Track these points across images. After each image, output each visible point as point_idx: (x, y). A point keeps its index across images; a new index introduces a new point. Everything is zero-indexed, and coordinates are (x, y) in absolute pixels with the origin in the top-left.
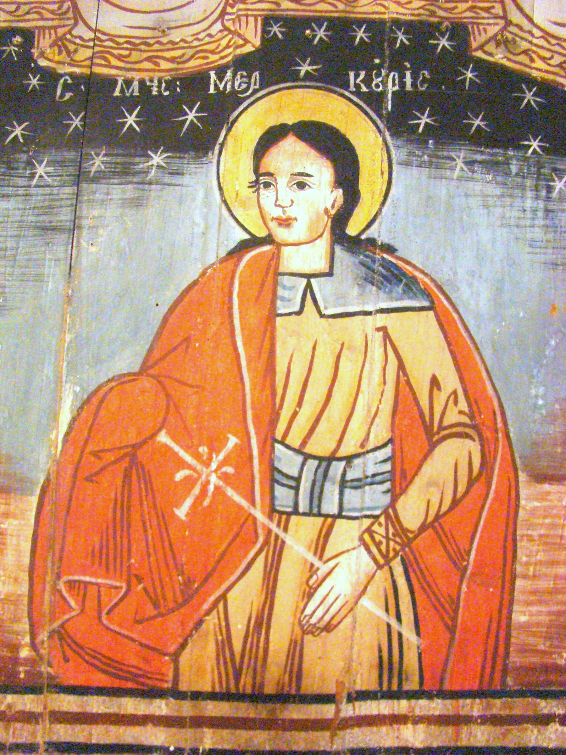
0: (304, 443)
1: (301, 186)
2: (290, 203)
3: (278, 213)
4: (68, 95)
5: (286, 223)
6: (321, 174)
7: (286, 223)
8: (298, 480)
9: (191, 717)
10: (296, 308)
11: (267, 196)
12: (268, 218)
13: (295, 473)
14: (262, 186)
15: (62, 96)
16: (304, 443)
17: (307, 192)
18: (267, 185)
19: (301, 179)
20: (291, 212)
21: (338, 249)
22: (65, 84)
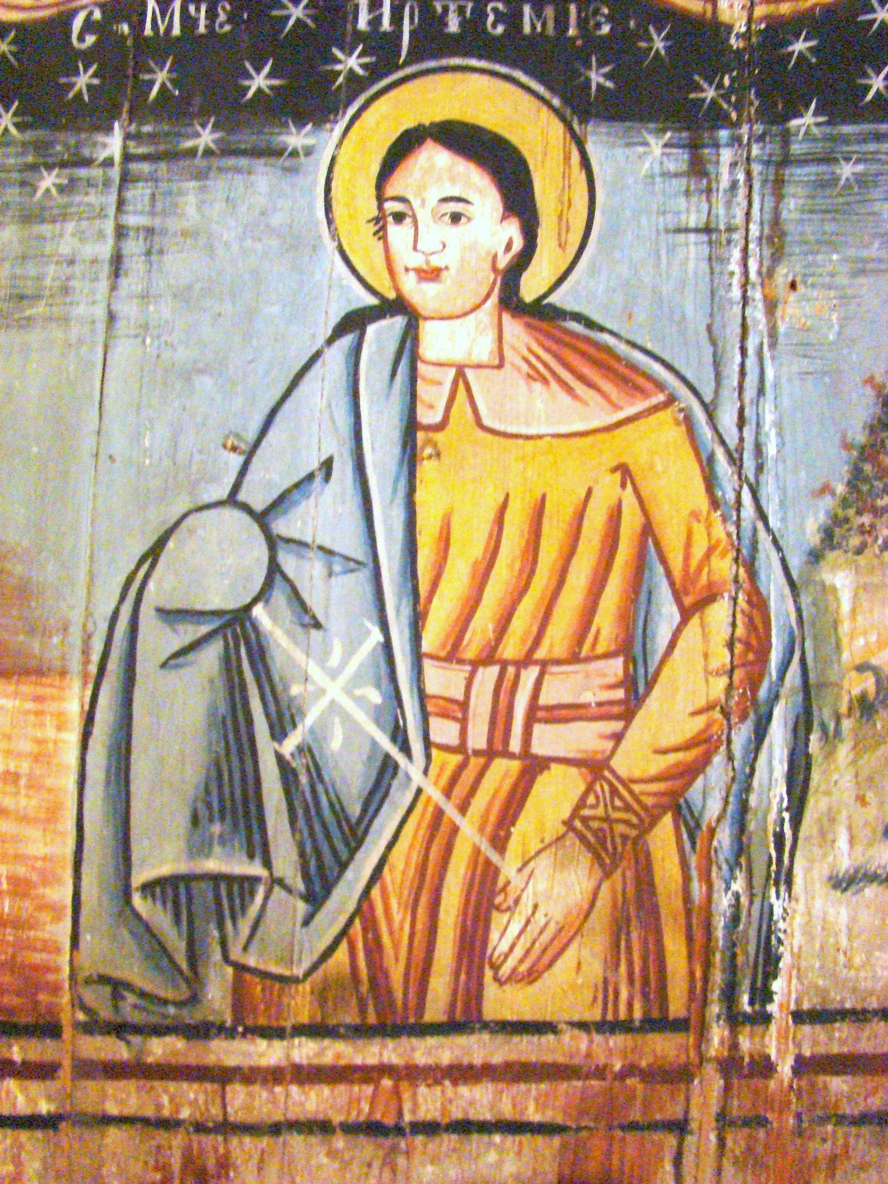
0: (281, 502)
1: (456, 218)
2: (441, 247)
3: (417, 261)
4: (90, 40)
5: (431, 274)
6: (151, 266)
7: (431, 274)
8: (464, 705)
9: (233, 1038)
10: (487, 422)
11: (398, 234)
12: (399, 268)
13: (461, 697)
14: (390, 219)
15: (81, 39)
16: (281, 502)
17: (462, 228)
18: (399, 218)
19: (453, 207)
20: (436, 261)
21: (506, 317)
22: (88, 22)
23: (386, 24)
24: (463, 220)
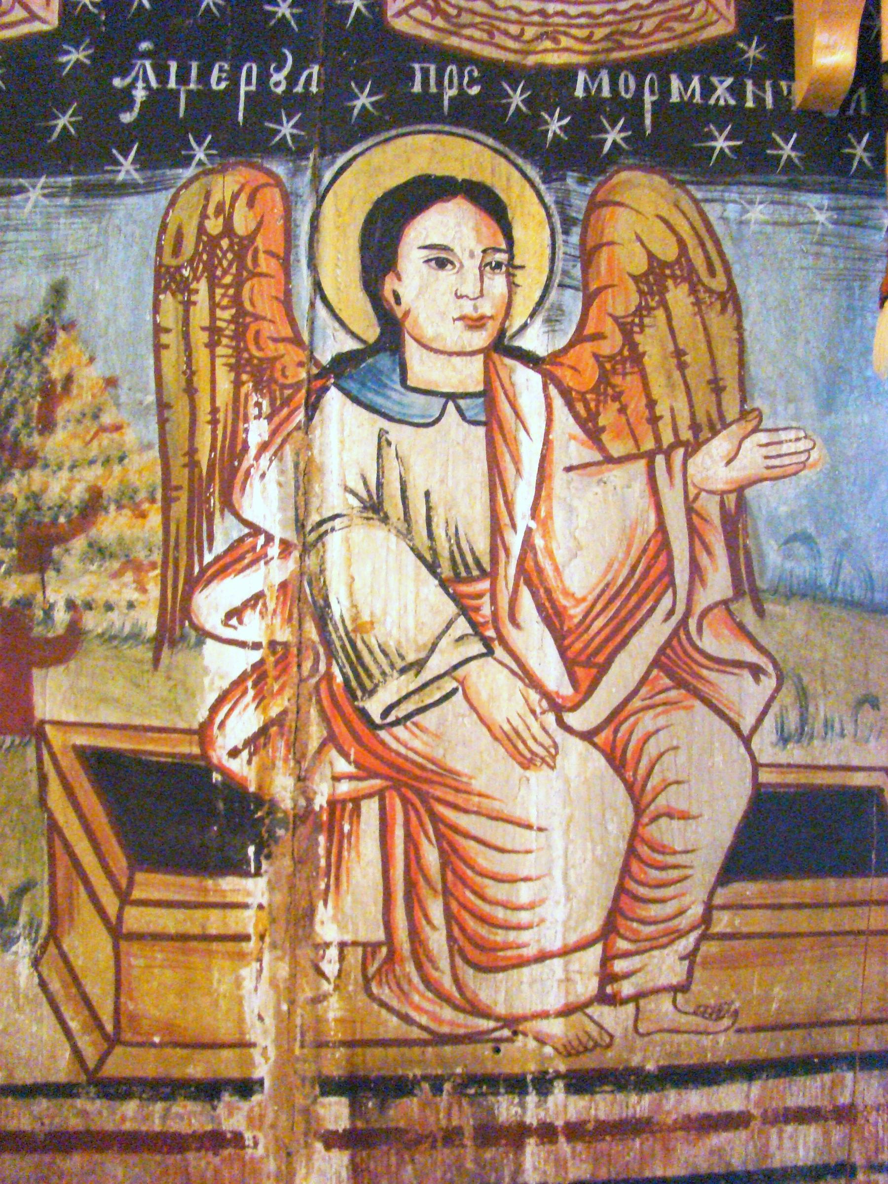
23: (433, 89)
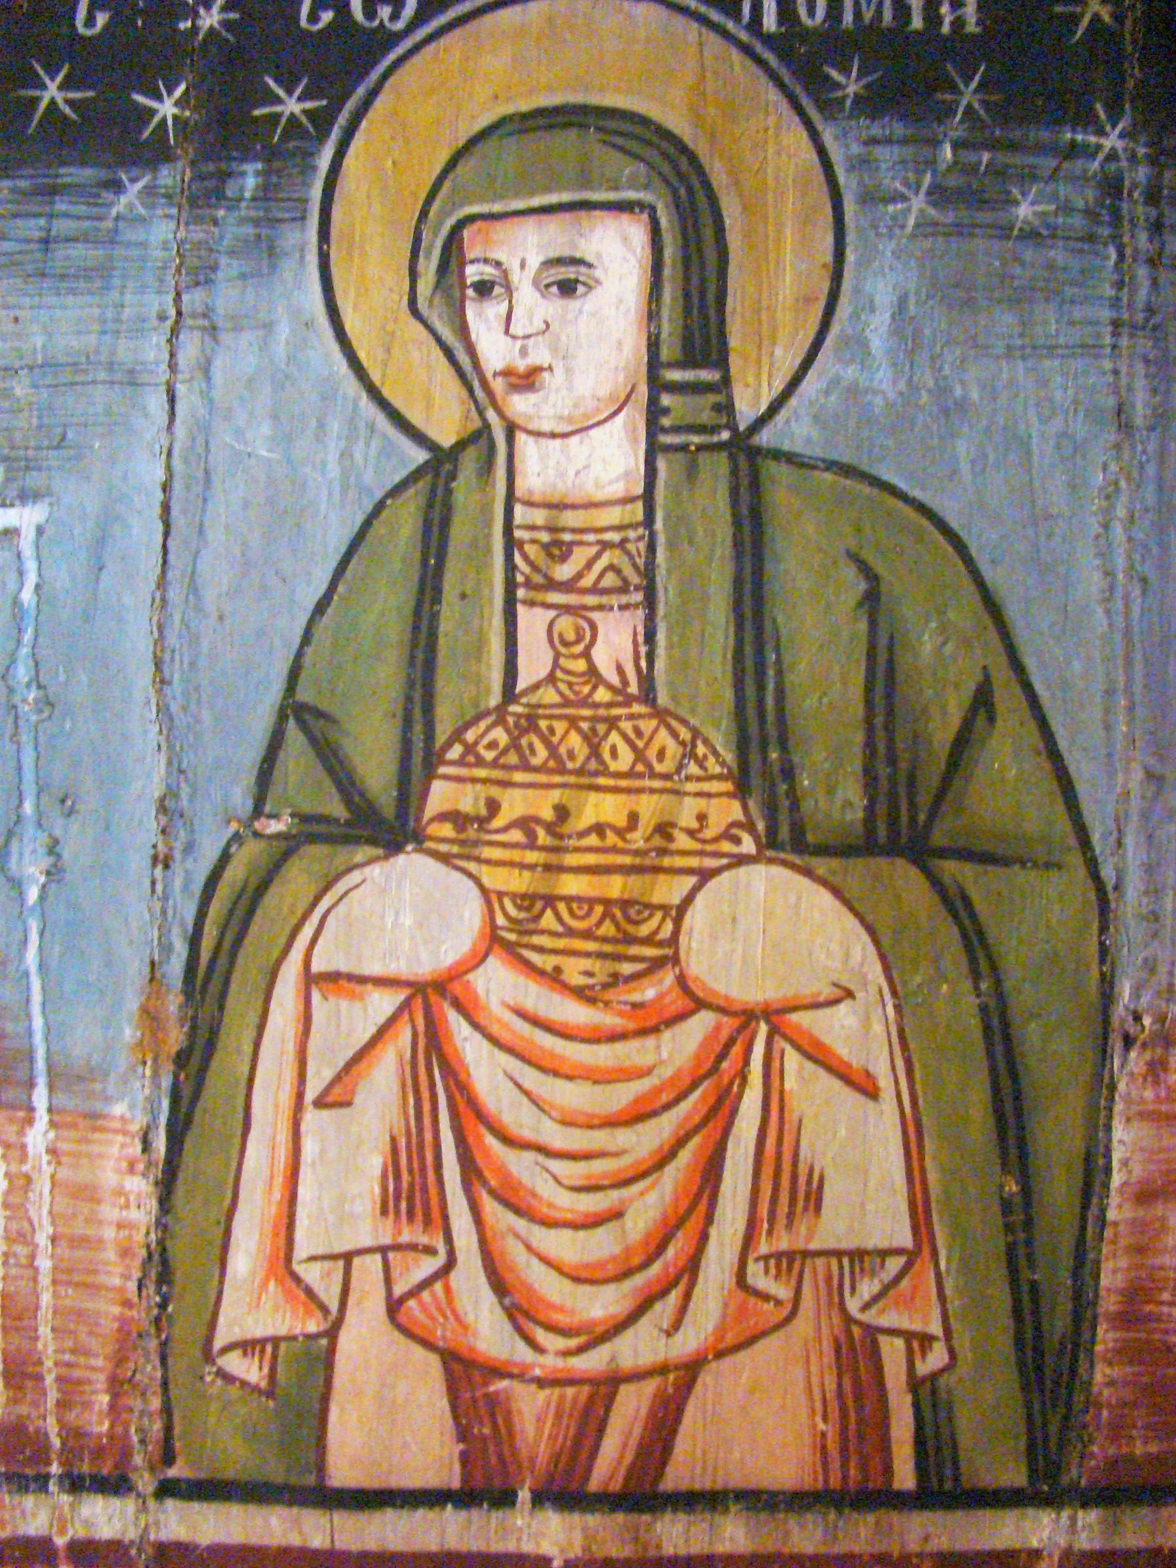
20: (540, 355)
24: (581, 289)
